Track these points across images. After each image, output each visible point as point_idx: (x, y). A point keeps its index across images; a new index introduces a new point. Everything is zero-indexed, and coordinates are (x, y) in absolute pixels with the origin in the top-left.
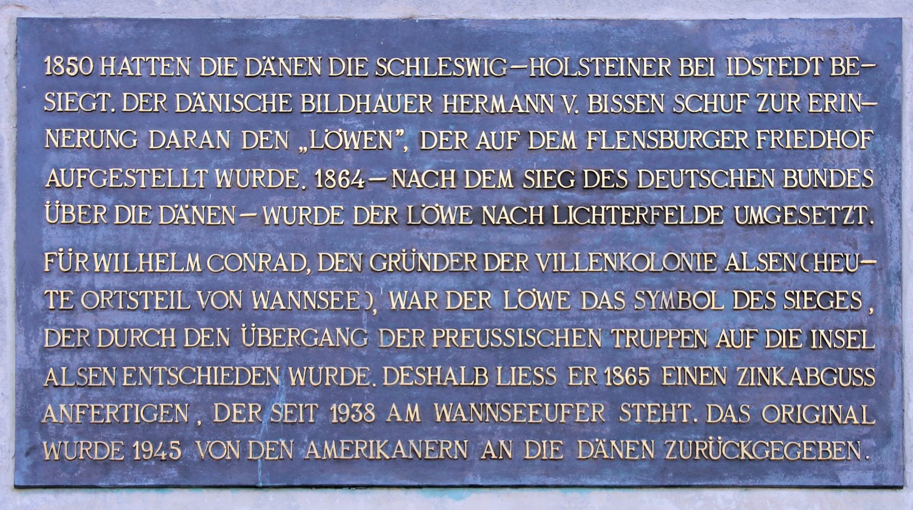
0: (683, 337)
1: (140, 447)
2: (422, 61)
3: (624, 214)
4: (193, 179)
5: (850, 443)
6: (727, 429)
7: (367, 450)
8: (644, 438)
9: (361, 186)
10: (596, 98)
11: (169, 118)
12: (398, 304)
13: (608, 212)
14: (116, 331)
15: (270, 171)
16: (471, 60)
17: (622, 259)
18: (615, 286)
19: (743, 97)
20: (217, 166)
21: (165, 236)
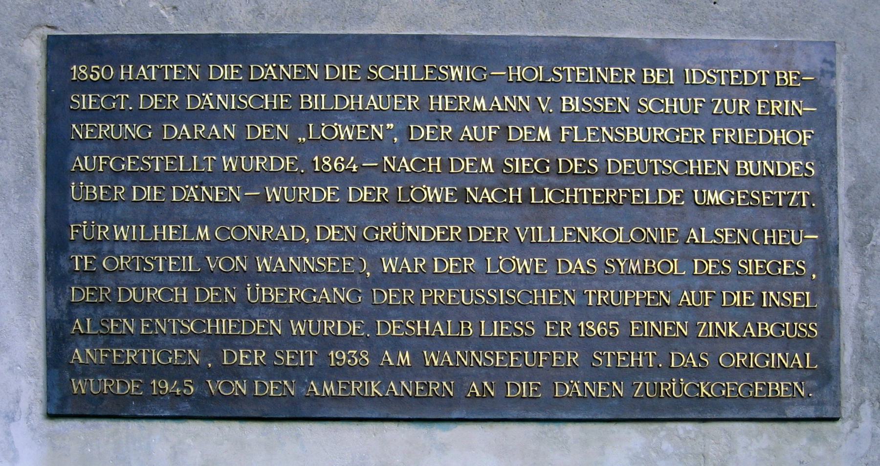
0: (649, 297)
1: (157, 385)
2: (410, 68)
3: (595, 195)
4: (202, 165)
5: (796, 384)
6: (688, 372)
7: (363, 389)
8: (614, 380)
9: (354, 170)
10: (568, 100)
11: (180, 115)
12: (390, 268)
13: (581, 194)
14: (134, 289)
15: (272, 158)
16: (454, 68)
17: (594, 233)
18: (587, 254)
19: (700, 101)
20: (223, 154)
21: (177, 211)
